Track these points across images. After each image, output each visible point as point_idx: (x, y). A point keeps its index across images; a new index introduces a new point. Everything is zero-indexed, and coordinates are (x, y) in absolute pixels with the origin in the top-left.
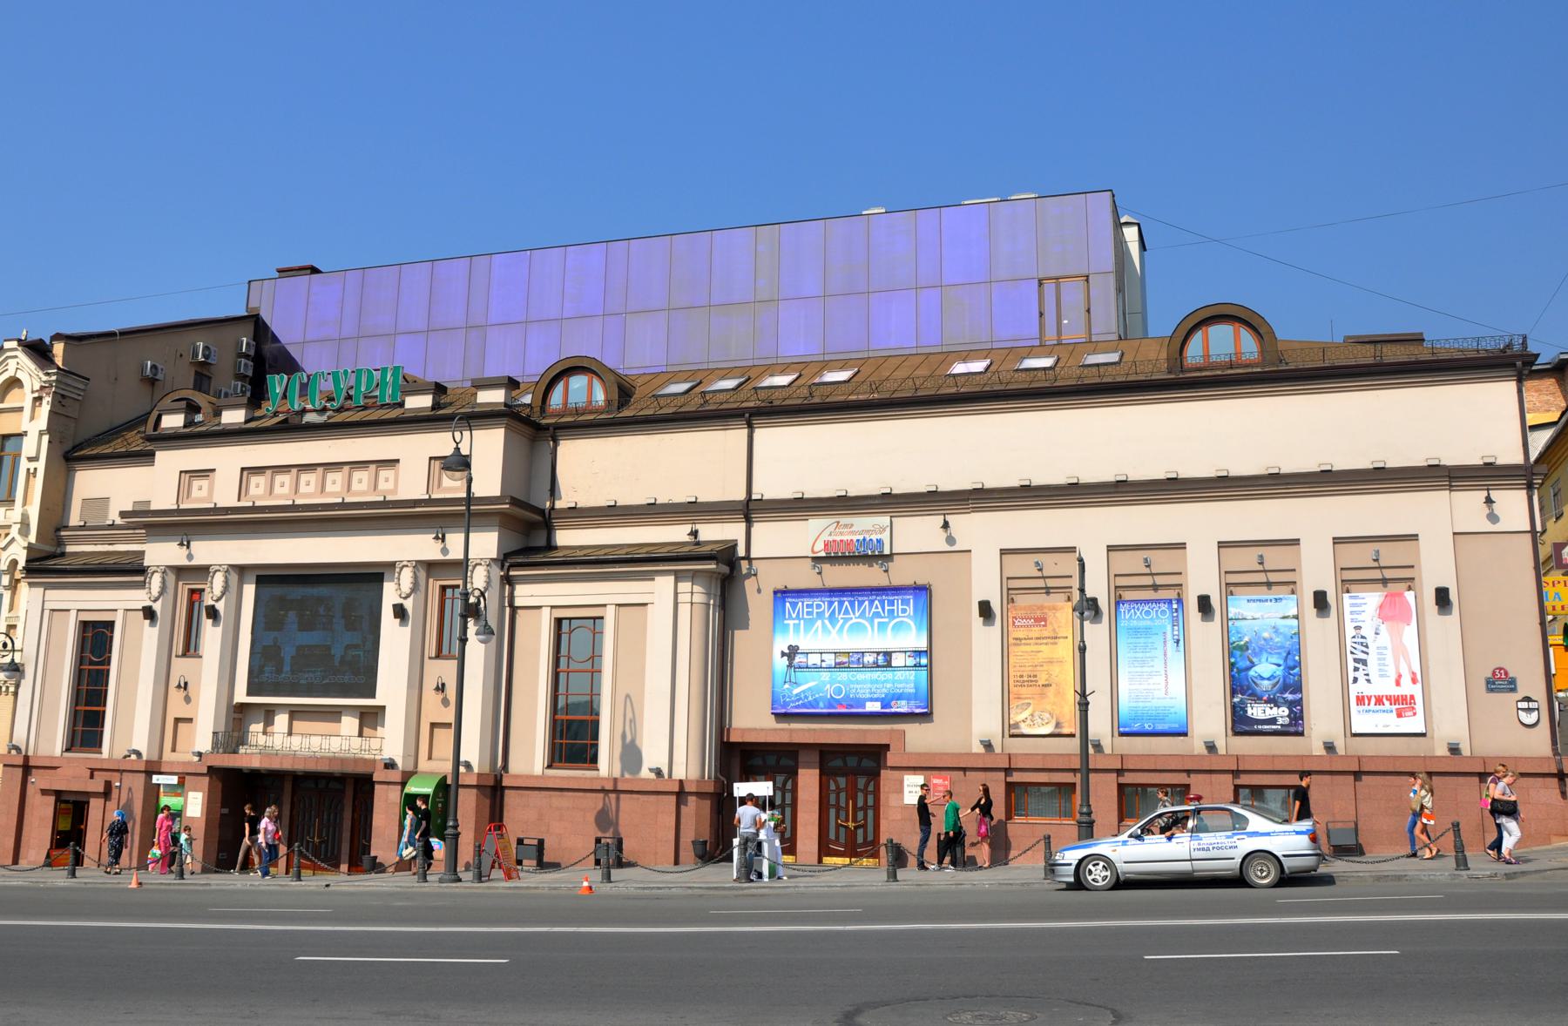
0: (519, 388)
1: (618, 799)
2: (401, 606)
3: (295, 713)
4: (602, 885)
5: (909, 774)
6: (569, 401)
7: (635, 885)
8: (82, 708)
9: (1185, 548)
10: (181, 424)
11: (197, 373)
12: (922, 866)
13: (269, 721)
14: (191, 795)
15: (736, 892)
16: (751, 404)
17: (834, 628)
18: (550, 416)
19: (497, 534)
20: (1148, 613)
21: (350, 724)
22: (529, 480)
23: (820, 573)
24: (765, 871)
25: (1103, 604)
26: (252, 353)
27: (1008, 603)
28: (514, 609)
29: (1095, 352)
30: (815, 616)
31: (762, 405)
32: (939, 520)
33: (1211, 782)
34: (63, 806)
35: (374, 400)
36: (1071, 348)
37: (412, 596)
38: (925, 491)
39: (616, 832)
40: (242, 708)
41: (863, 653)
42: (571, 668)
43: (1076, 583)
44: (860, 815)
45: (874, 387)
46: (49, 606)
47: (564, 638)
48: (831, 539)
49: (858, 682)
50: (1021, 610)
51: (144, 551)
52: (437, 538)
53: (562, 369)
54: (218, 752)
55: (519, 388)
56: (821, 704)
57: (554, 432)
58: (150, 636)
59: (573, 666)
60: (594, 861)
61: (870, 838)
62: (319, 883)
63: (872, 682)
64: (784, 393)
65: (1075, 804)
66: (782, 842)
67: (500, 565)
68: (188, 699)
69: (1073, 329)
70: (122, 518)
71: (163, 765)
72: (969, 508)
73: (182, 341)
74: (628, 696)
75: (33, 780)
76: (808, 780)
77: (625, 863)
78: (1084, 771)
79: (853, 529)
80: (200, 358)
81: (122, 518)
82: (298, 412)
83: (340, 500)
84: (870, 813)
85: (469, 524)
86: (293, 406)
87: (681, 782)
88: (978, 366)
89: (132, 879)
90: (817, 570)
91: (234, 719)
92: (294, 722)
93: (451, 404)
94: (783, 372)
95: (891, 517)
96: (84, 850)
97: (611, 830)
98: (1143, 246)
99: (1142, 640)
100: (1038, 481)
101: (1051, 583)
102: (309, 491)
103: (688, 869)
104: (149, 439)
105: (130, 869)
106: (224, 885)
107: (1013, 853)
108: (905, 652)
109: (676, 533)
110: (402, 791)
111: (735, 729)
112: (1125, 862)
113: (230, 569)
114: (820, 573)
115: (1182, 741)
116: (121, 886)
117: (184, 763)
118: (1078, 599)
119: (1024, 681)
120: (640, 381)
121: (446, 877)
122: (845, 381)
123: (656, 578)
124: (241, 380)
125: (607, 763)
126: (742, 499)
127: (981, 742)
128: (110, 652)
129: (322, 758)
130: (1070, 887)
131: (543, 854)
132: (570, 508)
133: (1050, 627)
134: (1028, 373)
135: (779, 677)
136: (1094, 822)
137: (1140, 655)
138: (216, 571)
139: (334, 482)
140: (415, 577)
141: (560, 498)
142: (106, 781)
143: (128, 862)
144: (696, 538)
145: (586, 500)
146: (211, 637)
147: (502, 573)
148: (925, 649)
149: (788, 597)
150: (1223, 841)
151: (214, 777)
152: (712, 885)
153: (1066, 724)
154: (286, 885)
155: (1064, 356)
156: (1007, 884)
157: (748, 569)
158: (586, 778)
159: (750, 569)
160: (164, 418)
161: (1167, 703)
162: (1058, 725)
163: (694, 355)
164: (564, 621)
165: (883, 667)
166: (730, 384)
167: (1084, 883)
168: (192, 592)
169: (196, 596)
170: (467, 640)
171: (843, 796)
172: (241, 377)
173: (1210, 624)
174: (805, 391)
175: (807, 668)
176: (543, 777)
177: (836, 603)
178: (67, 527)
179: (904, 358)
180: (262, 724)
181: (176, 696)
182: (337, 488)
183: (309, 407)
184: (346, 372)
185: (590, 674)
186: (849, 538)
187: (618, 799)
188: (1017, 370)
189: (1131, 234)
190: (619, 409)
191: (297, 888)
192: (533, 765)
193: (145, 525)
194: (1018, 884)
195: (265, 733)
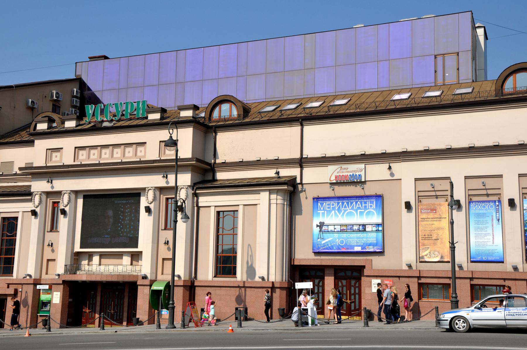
0: (199, 110)
1: (245, 290)
2: (149, 207)
3: (102, 256)
4: (238, 329)
5: (374, 279)
7: (252, 328)
9: (502, 177)
11: (53, 105)
12: (380, 320)
14: (55, 293)
15: (296, 331)
16: (302, 115)
17: (340, 214)
18: (213, 122)
19: (190, 174)
20: (484, 207)
21: (126, 260)
22: (204, 150)
23: (333, 190)
24: (310, 322)
25: (463, 203)
26: (79, 95)
27: (418, 203)
29: (460, 88)
30: (331, 209)
31: (307, 115)
32: (387, 166)
33: (516, 284)
35: (134, 116)
36: (449, 86)
38: (381, 153)
39: (245, 305)
40: (78, 254)
41: (353, 225)
42: (224, 233)
43: (449, 193)
44: (353, 297)
45: (357, 106)
47: (221, 220)
48: (338, 175)
49: (351, 238)
50: (424, 205)
51: (31, 185)
52: (164, 177)
53: (218, 101)
54: (67, 274)
55: (199, 110)
56: (335, 248)
57: (215, 129)
58: (35, 223)
59: (225, 232)
60: (235, 318)
61: (357, 307)
62: (112, 331)
63: (357, 238)
64: (317, 110)
65: (450, 293)
66: (317, 309)
67: (192, 188)
68: (53, 251)
69: (451, 77)
70: (20, 170)
71: (42, 280)
72: (400, 160)
73: (46, 90)
74: (249, 245)
76: (329, 281)
77: (249, 319)
78: (453, 278)
79: (348, 170)
80: (55, 98)
81: (20, 170)
82: (100, 122)
83: (120, 161)
84: (357, 296)
85: (177, 170)
86: (97, 119)
87: (273, 282)
88: (405, 96)
89: (26, 332)
90: (332, 189)
91: (74, 259)
92: (102, 259)
93: (169, 117)
94: (316, 101)
95: (365, 164)
96: (4, 321)
97: (243, 304)
98: (486, 37)
99: (481, 219)
100: (432, 147)
101: (438, 193)
102: (106, 157)
103: (276, 321)
104: (31, 135)
105: (26, 328)
106: (69, 333)
107: (422, 315)
108: (372, 224)
109: (269, 173)
111: (296, 259)
112: (473, 320)
113: (71, 192)
114: (333, 190)
115: (501, 265)
116: (21, 336)
117: (52, 279)
118: (450, 200)
119: (426, 238)
120: (253, 106)
122: (344, 104)
123: (261, 193)
124: (74, 108)
125: (241, 275)
126: (299, 157)
127: (406, 264)
128: (16, 231)
129: (114, 275)
130: (448, 330)
132: (222, 163)
133: (438, 213)
134: (428, 99)
135: (315, 237)
136: (458, 301)
137: (481, 226)
138: (65, 193)
140: (155, 194)
141: (218, 158)
144: (278, 175)
145: (230, 159)
146: (63, 222)
147: (193, 192)
148: (381, 223)
149: (319, 201)
150: (521, 311)
151: (65, 285)
152: (286, 328)
153: (446, 257)
154: (97, 332)
155: (445, 91)
156: (418, 329)
157: (301, 188)
158: (231, 281)
159: (302, 188)
160: (38, 125)
161: (494, 248)
162: (442, 257)
163: (277, 94)
164: (220, 212)
165: (362, 231)
166: (293, 106)
167: (454, 329)
168: (54, 203)
169: (56, 205)
170: (177, 221)
171: (345, 288)
172: (74, 107)
173: (514, 212)
174: (326, 109)
175: (328, 232)
176: (212, 281)
177: (341, 203)
179: (371, 93)
180: (87, 261)
181: (47, 250)
182: (119, 155)
183: (105, 119)
184: (121, 103)
185: (232, 235)
186: (346, 174)
187: (245, 290)
188: (423, 97)
189: (480, 32)
190: (243, 118)
191: (102, 333)
192: (208, 276)
193: (31, 174)
194: (423, 329)
195: (88, 265)
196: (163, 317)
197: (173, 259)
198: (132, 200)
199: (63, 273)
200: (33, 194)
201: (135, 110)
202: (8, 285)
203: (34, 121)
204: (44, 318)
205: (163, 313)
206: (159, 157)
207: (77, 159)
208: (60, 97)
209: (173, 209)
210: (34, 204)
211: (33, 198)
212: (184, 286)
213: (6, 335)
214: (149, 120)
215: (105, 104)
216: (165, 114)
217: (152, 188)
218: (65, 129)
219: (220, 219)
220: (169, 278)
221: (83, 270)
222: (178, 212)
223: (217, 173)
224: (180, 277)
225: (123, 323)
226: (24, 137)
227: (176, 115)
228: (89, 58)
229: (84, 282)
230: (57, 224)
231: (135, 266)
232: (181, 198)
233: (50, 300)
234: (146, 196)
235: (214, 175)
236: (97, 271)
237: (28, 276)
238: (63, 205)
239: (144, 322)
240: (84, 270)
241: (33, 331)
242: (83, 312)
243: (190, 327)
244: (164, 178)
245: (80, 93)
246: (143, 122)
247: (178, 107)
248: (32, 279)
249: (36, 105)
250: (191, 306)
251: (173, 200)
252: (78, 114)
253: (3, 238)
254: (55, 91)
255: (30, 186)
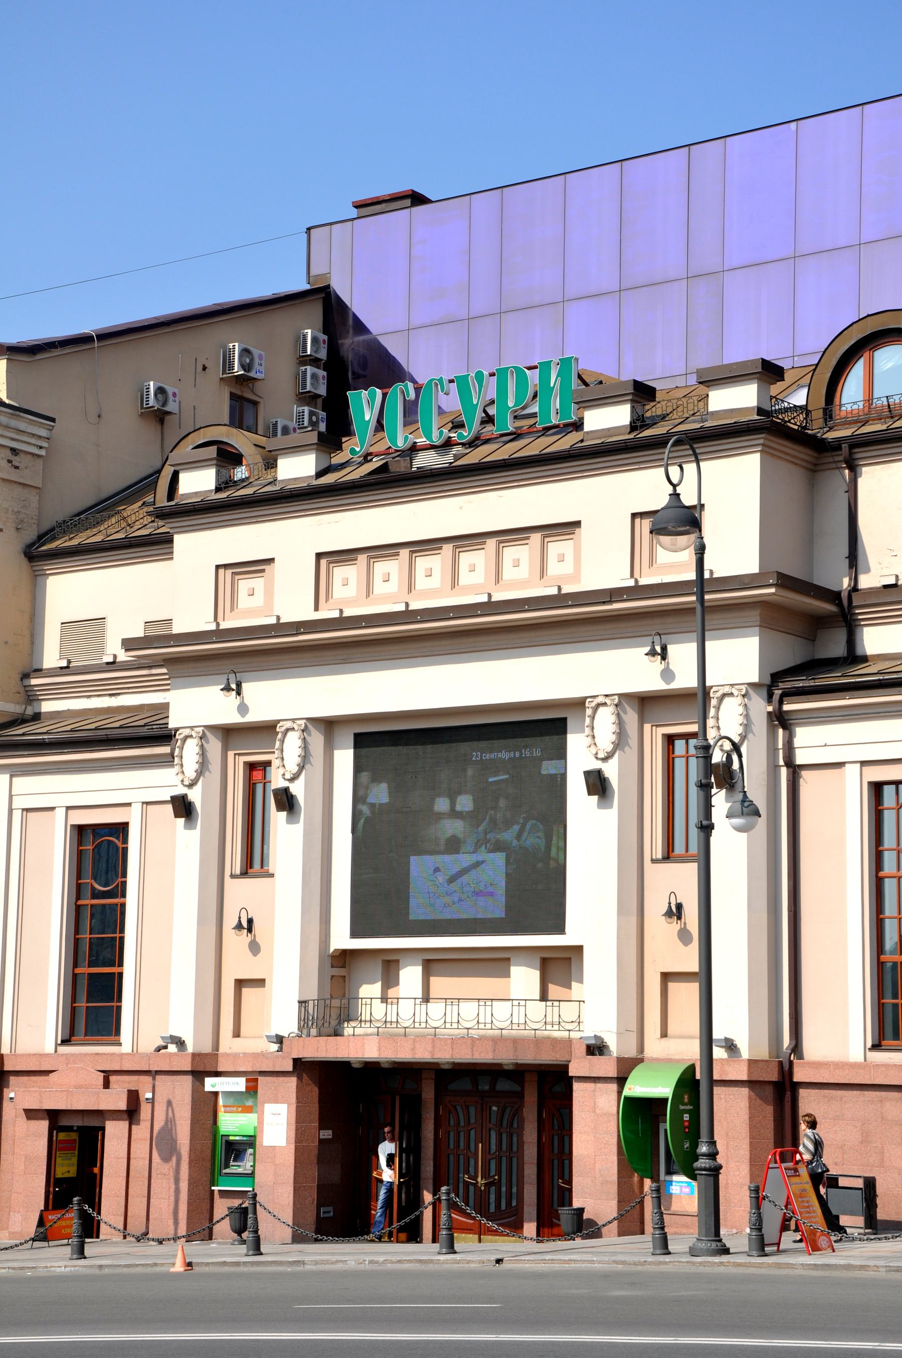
0: (783, 380)
2: (599, 773)
6: (876, 394)
8: (83, 970)
10: (212, 486)
11: (233, 396)
13: (390, 978)
26: (323, 354)
28: (795, 770)
34: (62, 1136)
35: (531, 421)
37: (617, 755)
40: (345, 957)
46: (19, 803)
52: (652, 653)
54: (309, 1035)
55: (782, 379)
57: (851, 454)
62: (485, 1257)
68: (255, 948)
70: (127, 650)
71: (220, 1059)
75: (12, 1095)
80: (237, 370)
81: (127, 650)
82: (403, 451)
83: (484, 599)
86: (394, 440)
89: (175, 1256)
91: (333, 977)
93: (663, 417)
96: (99, 1213)
104: (162, 515)
105: (175, 1239)
110: (620, 1092)
113: (309, 726)
116: (158, 1269)
117: (255, 1056)
121: (702, 1245)
124: (308, 405)
128: (124, 875)
129: (482, 1038)
131: (876, 1206)
138: (288, 730)
139: (472, 569)
140: (620, 723)
141: (868, 570)
142: (130, 1092)
143: (172, 1228)
147: (770, 709)
154: (431, 1261)
160: (183, 477)
164: (886, 787)
168: (251, 767)
169: (258, 775)
170: (711, 827)
172: (308, 398)
176: (865, 1065)
178: (40, 670)
180: (379, 985)
181: (235, 943)
183: (422, 441)
184: (479, 375)
193: (164, 660)
195: (384, 999)
196: (675, 1207)
197: (703, 974)
198: (532, 749)
199: (296, 1030)
200: (177, 737)
201: (535, 396)
202: (107, 1077)
203: (168, 463)
204: (236, 1203)
205: (675, 1189)
206: (632, 575)
207: (327, 600)
208: (256, 366)
209: (694, 778)
210: (183, 772)
211: (177, 750)
212: (750, 1084)
213: (107, 1266)
214: (588, 433)
215: (420, 381)
216: (647, 407)
217: (608, 701)
218: (277, 488)
219: (886, 813)
220: (691, 1051)
221: (365, 1021)
222: (714, 791)
223: (866, 629)
224: (735, 1046)
225: (522, 1227)
226: (137, 523)
227: (691, 407)
228: (356, 207)
229: (371, 1068)
230: (265, 846)
231: (556, 1004)
232: (723, 734)
233: (253, 1134)
234: (587, 730)
235: (852, 641)
236: (417, 1025)
237: (172, 1043)
238: (284, 775)
239: (604, 1226)
240: (371, 1021)
241: (198, 1251)
242: (374, 1181)
243: (784, 1251)
244: (652, 659)
245: (326, 346)
246: (566, 442)
247: (699, 372)
248: (188, 1054)
249: (175, 401)
250: (783, 1165)
251: (693, 742)
252: (323, 427)
253: (80, 902)
254: (237, 344)
255: (164, 707)
